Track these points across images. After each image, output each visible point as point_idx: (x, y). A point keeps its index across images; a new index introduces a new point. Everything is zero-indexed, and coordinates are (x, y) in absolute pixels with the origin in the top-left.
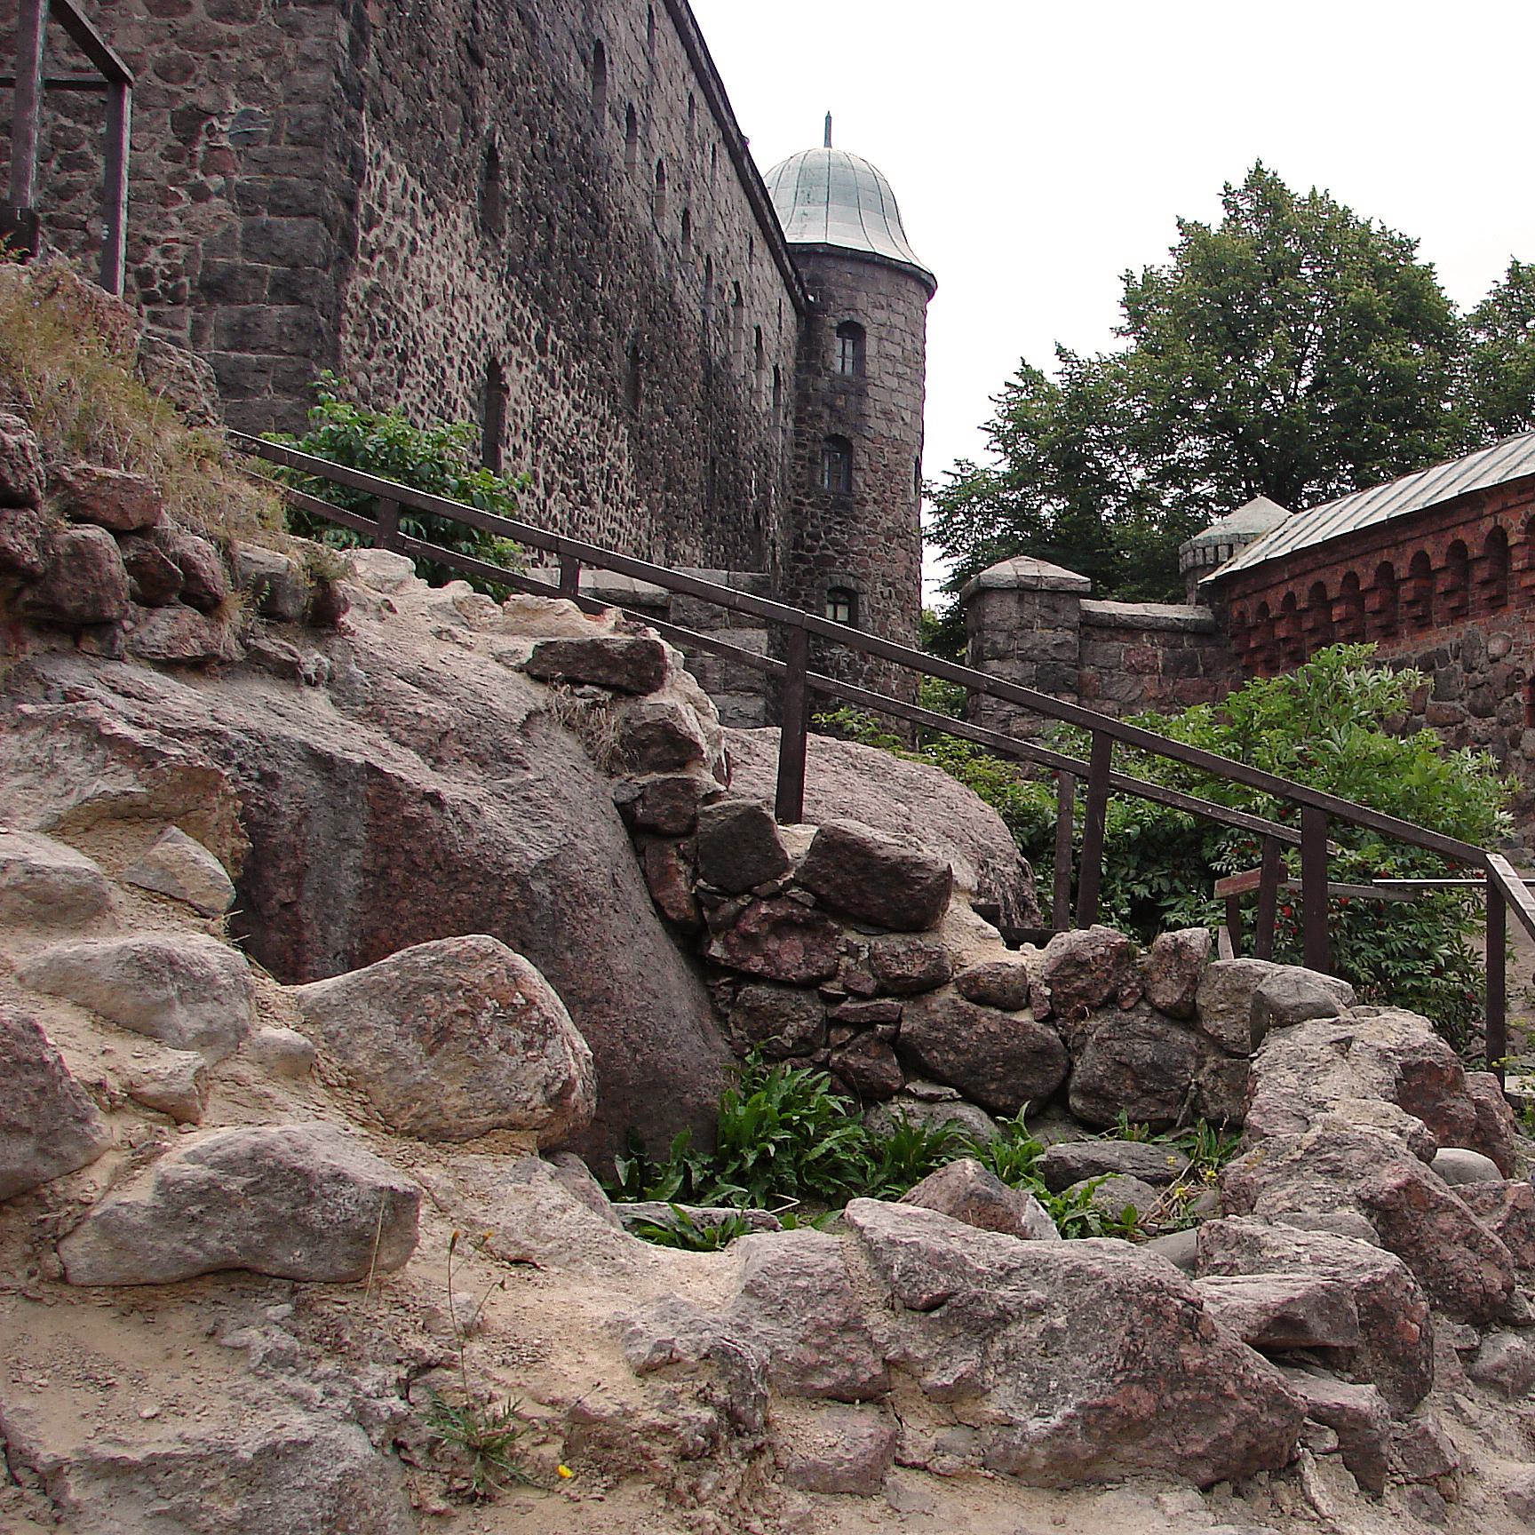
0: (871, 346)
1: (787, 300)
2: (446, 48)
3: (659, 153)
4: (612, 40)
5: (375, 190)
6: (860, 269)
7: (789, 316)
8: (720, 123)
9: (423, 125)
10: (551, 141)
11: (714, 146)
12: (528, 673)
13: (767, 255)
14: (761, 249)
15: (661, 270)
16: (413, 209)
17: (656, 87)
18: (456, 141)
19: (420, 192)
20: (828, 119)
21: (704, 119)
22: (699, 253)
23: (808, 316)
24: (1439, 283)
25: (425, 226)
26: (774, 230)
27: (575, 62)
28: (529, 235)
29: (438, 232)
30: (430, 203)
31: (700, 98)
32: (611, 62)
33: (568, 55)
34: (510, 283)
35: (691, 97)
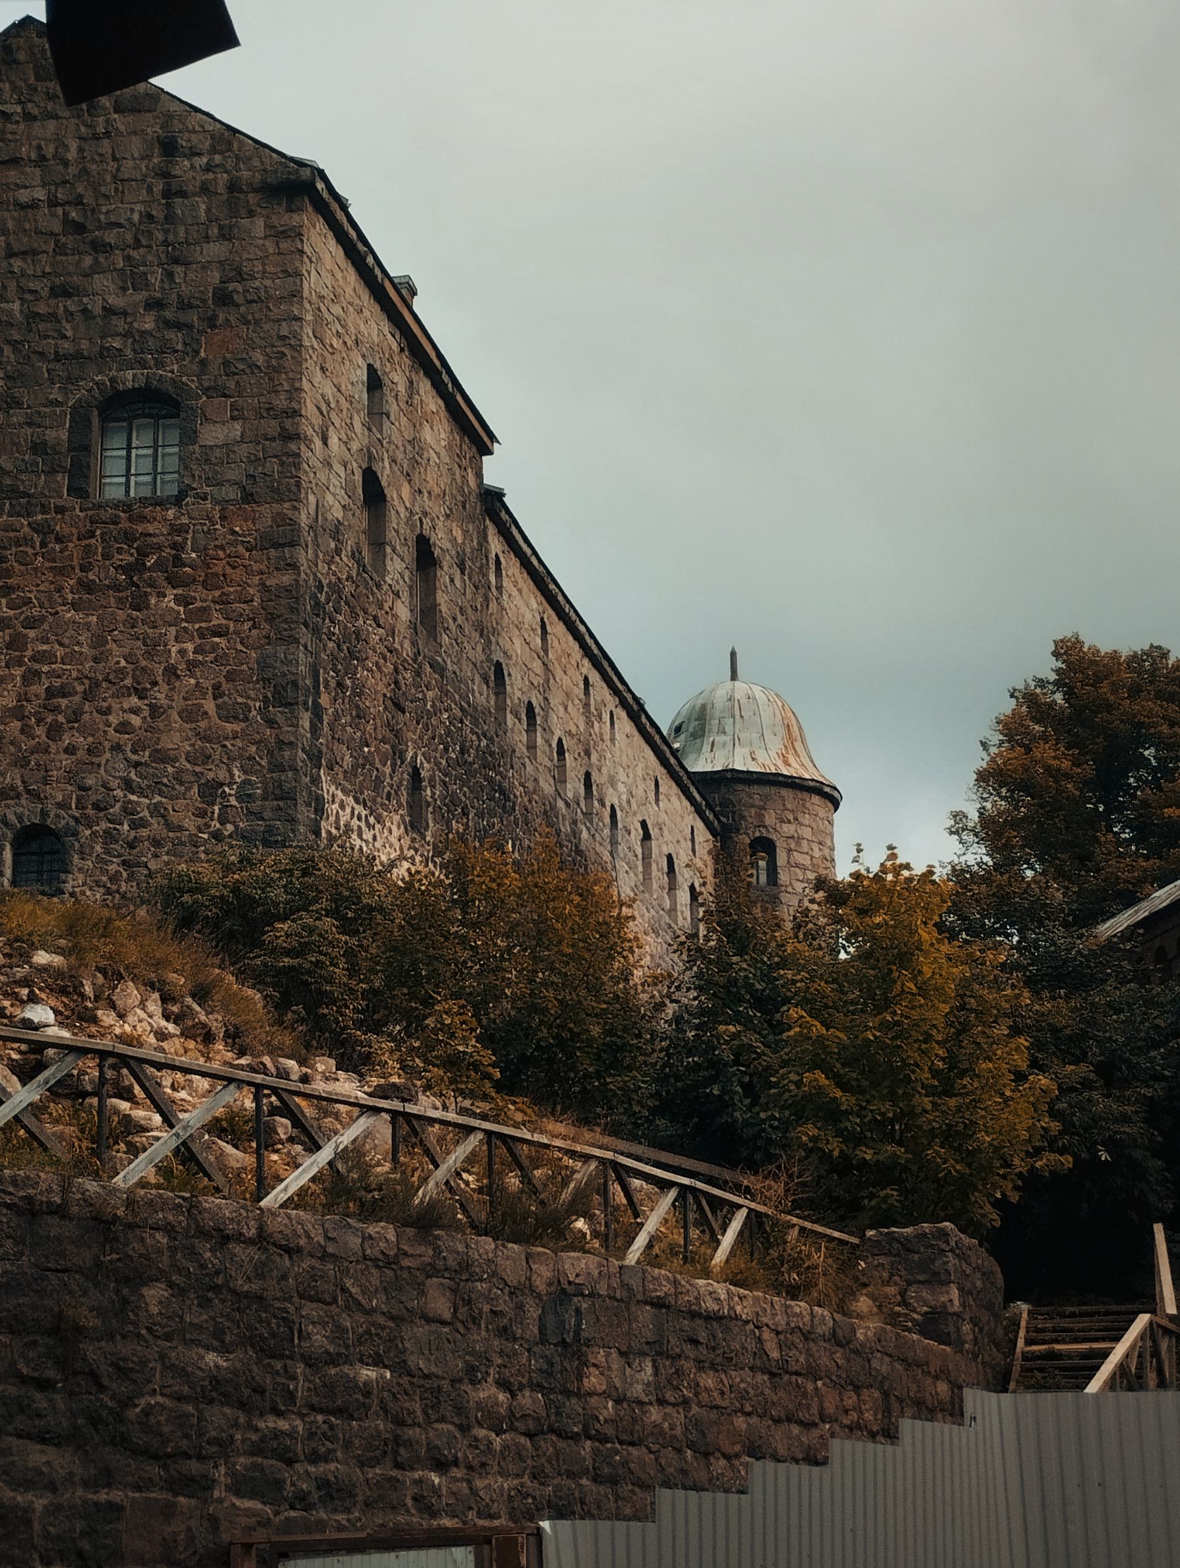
0: (781, 858)
1: (700, 825)
2: (375, 707)
3: (558, 733)
4: (509, 657)
5: (332, 819)
6: (767, 790)
7: (703, 835)
8: (615, 692)
9: (363, 766)
10: (462, 752)
11: (611, 713)
12: (919, 1403)
13: (675, 789)
14: (668, 787)
15: (566, 828)
16: (359, 827)
17: (552, 681)
18: (388, 770)
19: (364, 813)
20: (733, 655)
21: (601, 691)
22: (603, 805)
23: (723, 834)
24: (919, 869)
25: (368, 835)
26: (678, 769)
27: (478, 685)
28: (448, 822)
29: (378, 838)
30: (372, 820)
31: (595, 677)
32: (509, 675)
33: (472, 681)
34: (435, 863)
35: (586, 680)
